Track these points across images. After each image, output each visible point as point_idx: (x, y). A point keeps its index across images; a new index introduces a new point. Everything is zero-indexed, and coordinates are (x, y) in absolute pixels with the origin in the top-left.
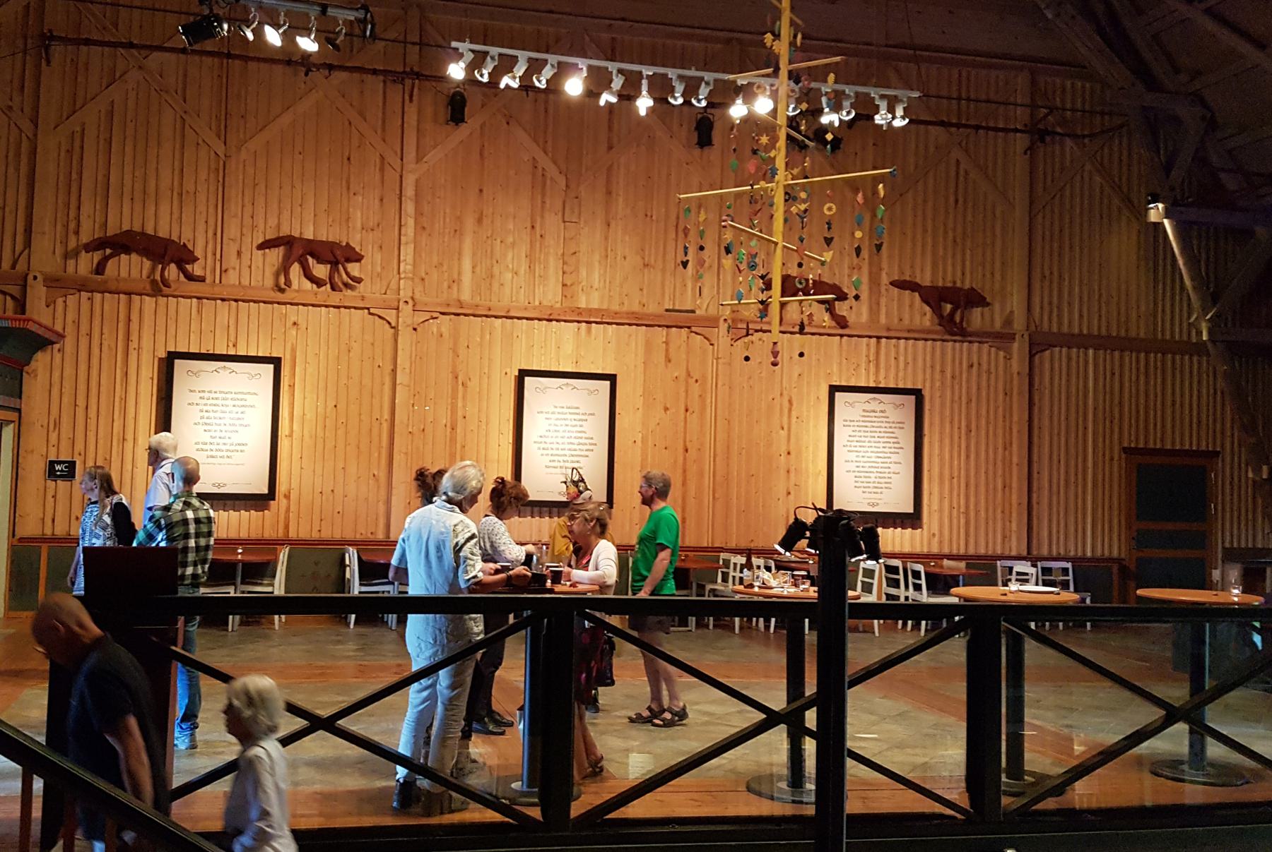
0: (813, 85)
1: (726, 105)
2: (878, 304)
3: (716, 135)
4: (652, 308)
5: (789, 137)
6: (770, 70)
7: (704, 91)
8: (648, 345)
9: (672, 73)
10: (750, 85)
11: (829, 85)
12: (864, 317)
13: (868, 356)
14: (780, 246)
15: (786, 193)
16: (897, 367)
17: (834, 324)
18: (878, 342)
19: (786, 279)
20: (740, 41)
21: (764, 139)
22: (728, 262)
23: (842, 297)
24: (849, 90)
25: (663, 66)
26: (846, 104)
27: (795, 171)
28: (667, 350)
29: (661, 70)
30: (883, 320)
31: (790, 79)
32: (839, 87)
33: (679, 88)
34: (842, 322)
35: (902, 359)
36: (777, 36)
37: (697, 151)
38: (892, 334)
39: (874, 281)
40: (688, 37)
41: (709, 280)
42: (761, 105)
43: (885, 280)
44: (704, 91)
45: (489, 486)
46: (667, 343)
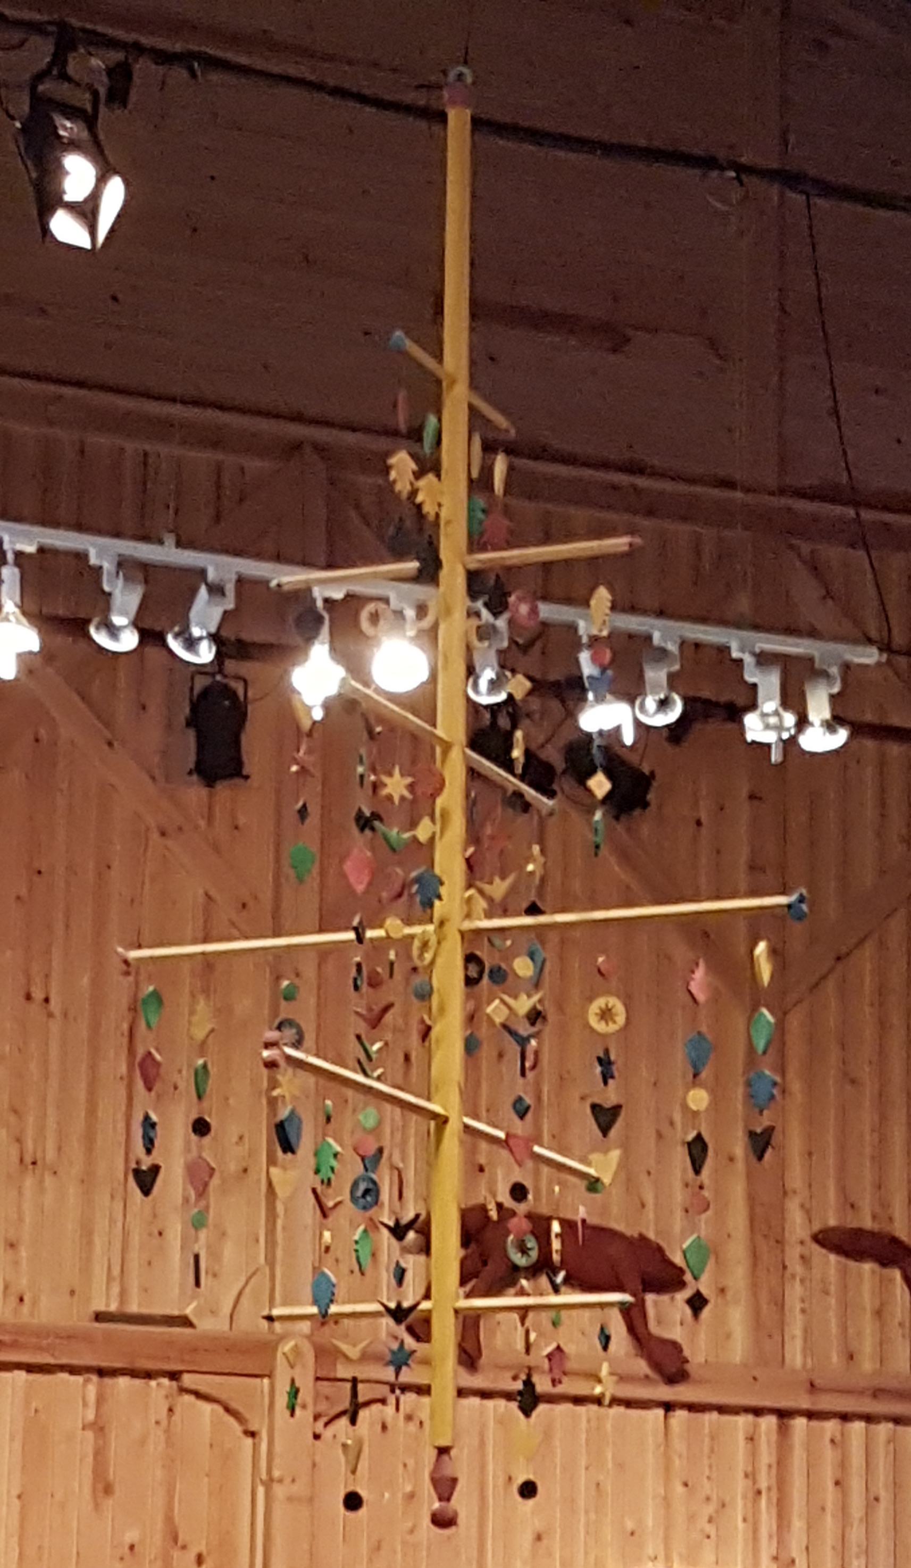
0: (547, 611)
1: (285, 652)
2: (780, 1304)
3: (256, 746)
4: (49, 1310)
5: (473, 773)
6: (412, 565)
7: (205, 615)
8: (35, 1440)
9: (101, 551)
10: (353, 601)
11: (597, 617)
12: (738, 1348)
13: (751, 1475)
14: (452, 1130)
15: (470, 958)
16: (844, 1508)
17: (642, 1366)
18: (783, 1431)
19: (477, 1230)
20: (320, 449)
21: (396, 785)
22: (293, 1176)
23: (662, 1276)
24: (664, 633)
25: (80, 527)
26: (656, 675)
27: (499, 888)
28: (99, 1454)
29: (64, 540)
30: (795, 1356)
31: (473, 593)
32: (632, 623)
33: (125, 602)
34: (669, 1364)
35: (856, 1485)
36: (429, 465)
37: (195, 793)
38: (826, 1403)
39: (766, 1227)
40: (163, 429)
41: (237, 1213)
42: (395, 656)
43: (798, 1226)
44: (205, 615)
45: (234, 577)
46: (99, 1428)
